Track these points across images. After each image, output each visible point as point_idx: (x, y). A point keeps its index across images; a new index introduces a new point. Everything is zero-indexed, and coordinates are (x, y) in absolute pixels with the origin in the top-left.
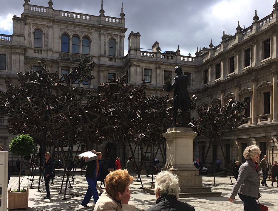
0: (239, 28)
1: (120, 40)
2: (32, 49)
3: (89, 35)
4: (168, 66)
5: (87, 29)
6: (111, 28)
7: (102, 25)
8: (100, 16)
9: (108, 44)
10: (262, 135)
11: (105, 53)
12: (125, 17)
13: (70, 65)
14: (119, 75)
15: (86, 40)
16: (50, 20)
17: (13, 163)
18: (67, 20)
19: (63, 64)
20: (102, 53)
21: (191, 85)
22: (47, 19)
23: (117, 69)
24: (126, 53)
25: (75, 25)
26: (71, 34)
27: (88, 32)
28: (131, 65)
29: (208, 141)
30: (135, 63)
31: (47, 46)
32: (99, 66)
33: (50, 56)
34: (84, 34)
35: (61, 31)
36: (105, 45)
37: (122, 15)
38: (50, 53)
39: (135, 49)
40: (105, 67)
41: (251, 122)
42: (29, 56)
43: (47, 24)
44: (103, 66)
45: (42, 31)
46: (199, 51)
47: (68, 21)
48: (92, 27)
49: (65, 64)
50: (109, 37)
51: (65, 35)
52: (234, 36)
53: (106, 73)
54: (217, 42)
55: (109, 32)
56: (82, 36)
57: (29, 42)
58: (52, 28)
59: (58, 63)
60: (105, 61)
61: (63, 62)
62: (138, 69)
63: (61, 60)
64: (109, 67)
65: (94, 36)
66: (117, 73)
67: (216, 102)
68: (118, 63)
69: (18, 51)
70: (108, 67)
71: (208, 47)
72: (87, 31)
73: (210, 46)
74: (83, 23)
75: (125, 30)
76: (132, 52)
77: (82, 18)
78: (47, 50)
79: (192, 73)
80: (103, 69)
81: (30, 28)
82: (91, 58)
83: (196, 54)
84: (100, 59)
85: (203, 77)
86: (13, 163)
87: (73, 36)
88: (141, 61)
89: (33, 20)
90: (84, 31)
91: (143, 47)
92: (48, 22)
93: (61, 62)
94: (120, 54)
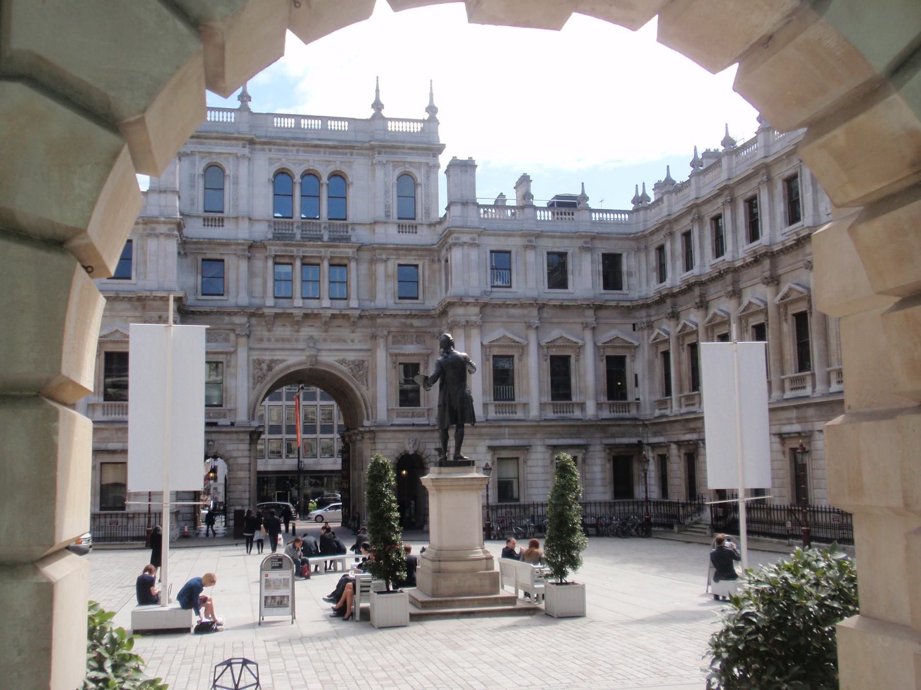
0: (728, 141)
1: (428, 178)
2: (199, 217)
3: (344, 169)
4: (557, 240)
5: (340, 153)
6: (403, 148)
7: (376, 141)
8: (374, 117)
9: (395, 189)
10: (796, 428)
11: (387, 215)
12: (438, 116)
13: (295, 251)
14: (427, 267)
15: (338, 180)
16: (243, 139)
17: (149, 518)
18: (287, 135)
19: (277, 251)
20: (380, 214)
21: (625, 287)
22: (236, 139)
23: (420, 253)
24: (442, 213)
25: (308, 146)
26: (297, 172)
27: (341, 162)
28: (455, 244)
29: (674, 442)
30: (466, 238)
31: (236, 206)
32: (373, 248)
33: (242, 232)
34: (332, 168)
35: (271, 164)
36: (387, 192)
37: (432, 109)
38: (244, 225)
39: (463, 200)
40: (390, 249)
41: (814, 386)
42: (190, 236)
43: (235, 151)
44: (383, 247)
45: (223, 170)
46: (640, 194)
47: (289, 139)
48: (353, 148)
49: (283, 248)
50: (398, 172)
51: (283, 173)
52: (683, 184)
53: (392, 266)
54: (681, 174)
55: (396, 158)
56: (325, 173)
57: (192, 200)
58: (249, 159)
59: (265, 247)
60: (390, 234)
61: (276, 245)
62: (474, 254)
63: (273, 239)
64: (399, 249)
65: (358, 170)
66: (420, 263)
67: (688, 334)
68: (425, 236)
69: (162, 229)
70: (397, 249)
71: (721, 149)
72: (339, 158)
73: (724, 143)
74: (329, 140)
75: (440, 149)
76: (457, 210)
77: (325, 128)
78: (237, 218)
79: (624, 256)
80: (384, 257)
81: (193, 164)
82: (350, 228)
83: (633, 202)
84: (374, 231)
85: (654, 264)
86: (149, 518)
87: (302, 177)
88: (482, 233)
89: (202, 144)
90: (330, 159)
91: (485, 194)
92: (237, 146)
93: (272, 245)
94: (428, 213)
